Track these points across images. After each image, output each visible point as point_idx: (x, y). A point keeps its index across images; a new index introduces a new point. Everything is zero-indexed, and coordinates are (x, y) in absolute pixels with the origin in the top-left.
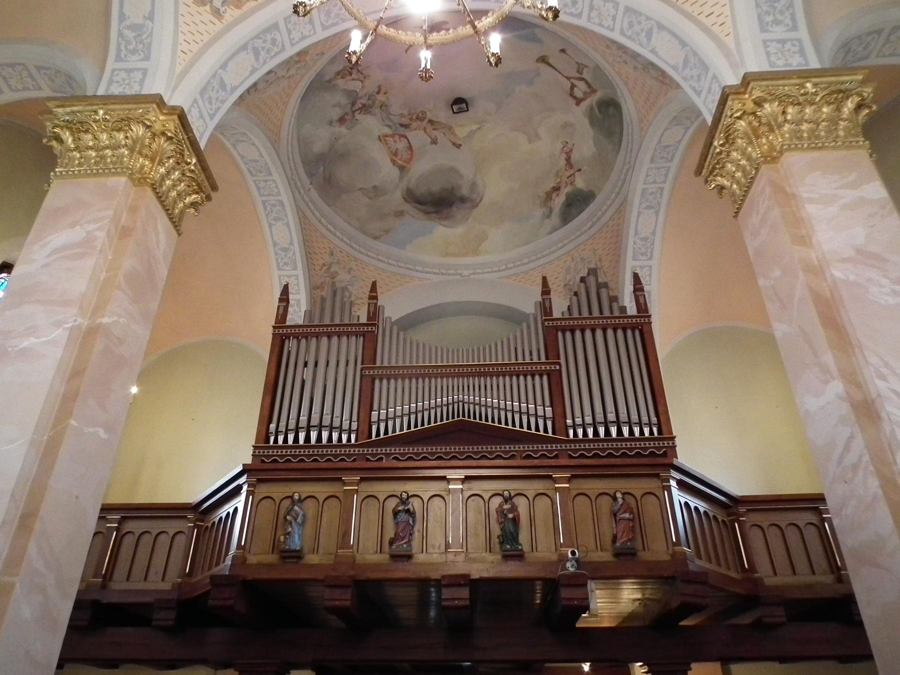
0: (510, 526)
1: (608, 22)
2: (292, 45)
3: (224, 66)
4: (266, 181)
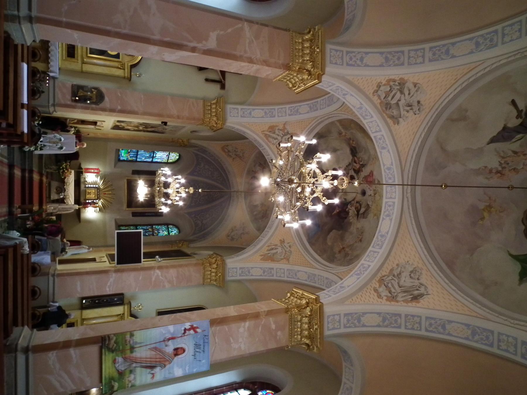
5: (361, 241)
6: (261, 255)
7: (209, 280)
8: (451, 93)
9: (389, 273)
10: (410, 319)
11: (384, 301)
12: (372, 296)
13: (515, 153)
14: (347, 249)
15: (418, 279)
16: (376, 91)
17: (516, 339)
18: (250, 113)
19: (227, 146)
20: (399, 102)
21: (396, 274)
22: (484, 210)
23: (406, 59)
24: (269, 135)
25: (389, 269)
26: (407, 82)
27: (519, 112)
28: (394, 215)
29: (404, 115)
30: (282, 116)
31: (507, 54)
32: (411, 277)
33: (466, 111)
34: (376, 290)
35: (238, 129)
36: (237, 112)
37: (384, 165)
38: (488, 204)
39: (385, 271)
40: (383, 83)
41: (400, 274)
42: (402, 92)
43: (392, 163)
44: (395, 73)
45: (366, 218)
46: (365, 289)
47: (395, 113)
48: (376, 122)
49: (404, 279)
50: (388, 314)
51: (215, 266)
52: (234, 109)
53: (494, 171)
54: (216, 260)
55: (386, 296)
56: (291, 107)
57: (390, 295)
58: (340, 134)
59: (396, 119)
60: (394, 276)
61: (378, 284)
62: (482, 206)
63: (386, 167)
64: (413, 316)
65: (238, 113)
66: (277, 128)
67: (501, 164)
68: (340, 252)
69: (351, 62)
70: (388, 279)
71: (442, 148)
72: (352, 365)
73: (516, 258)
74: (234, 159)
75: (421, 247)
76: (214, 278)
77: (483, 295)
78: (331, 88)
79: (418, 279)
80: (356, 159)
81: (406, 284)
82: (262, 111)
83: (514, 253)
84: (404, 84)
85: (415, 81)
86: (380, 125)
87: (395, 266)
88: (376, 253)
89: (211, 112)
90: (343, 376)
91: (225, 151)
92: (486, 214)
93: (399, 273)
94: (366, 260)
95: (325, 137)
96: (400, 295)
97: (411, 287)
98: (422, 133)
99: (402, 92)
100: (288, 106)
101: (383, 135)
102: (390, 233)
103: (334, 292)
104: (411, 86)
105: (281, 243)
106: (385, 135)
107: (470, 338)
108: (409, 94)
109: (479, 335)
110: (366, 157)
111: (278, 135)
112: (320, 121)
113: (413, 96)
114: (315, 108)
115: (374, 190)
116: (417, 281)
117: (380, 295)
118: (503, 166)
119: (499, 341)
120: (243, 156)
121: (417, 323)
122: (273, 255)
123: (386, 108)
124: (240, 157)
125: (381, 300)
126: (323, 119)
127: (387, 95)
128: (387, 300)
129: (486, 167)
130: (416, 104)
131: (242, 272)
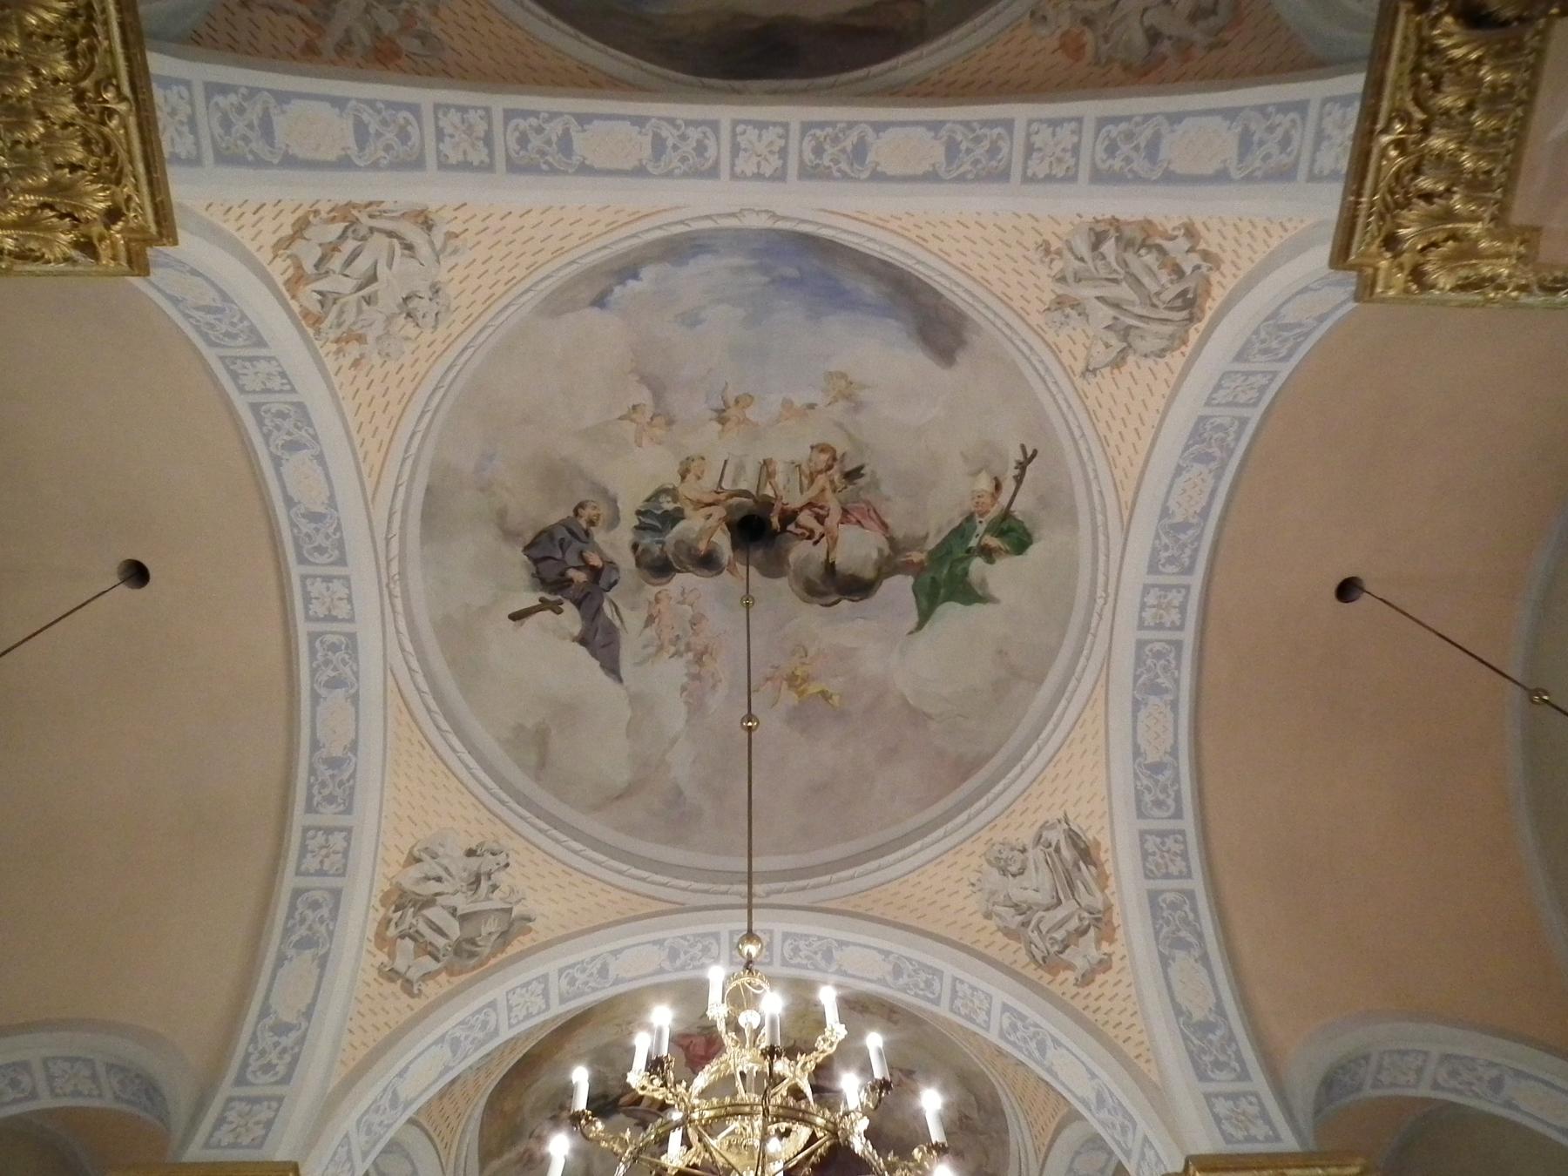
0: (128, 19)
1: (450, 120)
2: (1079, 120)
3: (1221, 177)
8: (462, 761)
9: (1018, 939)
10: (1157, 865)
11: (1118, 949)
12: (1108, 991)
13: (650, 620)
15: (1024, 851)
17: (1146, 589)
20: (459, 912)
21: (1020, 918)
22: (801, 694)
23: (335, 627)
25: (1006, 940)
26: (398, 885)
27: (544, 605)
28: (825, 932)
31: (382, 605)
32: (1021, 872)
34: (1086, 979)
37: (661, 971)
39: (1015, 953)
40: (385, 959)
41: (1016, 906)
42: (429, 902)
43: (654, 943)
44: (360, 914)
46: (1088, 1014)
47: (492, 926)
48: (513, 990)
49: (1030, 893)
50: (1157, 933)
53: (695, 669)
57: (1092, 933)
59: (513, 926)
60: (1025, 924)
61: (1062, 975)
62: (790, 698)
63: (667, 965)
64: (1145, 855)
67: (677, 654)
69: (281, 1069)
70: (1041, 945)
71: (618, 798)
72: (1367, 1058)
73: (925, 616)
75: (921, 849)
77: (1039, 680)
79: (1024, 851)
81: (1048, 886)
83: (914, 618)
84: (403, 893)
87: (991, 924)
88: (958, 986)
90: (1411, 1092)
92: (813, 688)
94: (988, 1023)
97: (1053, 870)
98: (568, 848)
99: (429, 902)
101: (561, 971)
102: (886, 945)
103: (1124, 1130)
104: (415, 872)
106: (562, 963)
107: (1169, 697)
108: (439, 879)
109: (1157, 676)
113: (446, 869)
116: (1030, 854)
117: (1101, 962)
118: (682, 648)
119: (1160, 626)
121: (1163, 843)
123: (472, 955)
125: (1115, 959)
128: (1111, 941)
129: (684, 689)
130: (473, 863)
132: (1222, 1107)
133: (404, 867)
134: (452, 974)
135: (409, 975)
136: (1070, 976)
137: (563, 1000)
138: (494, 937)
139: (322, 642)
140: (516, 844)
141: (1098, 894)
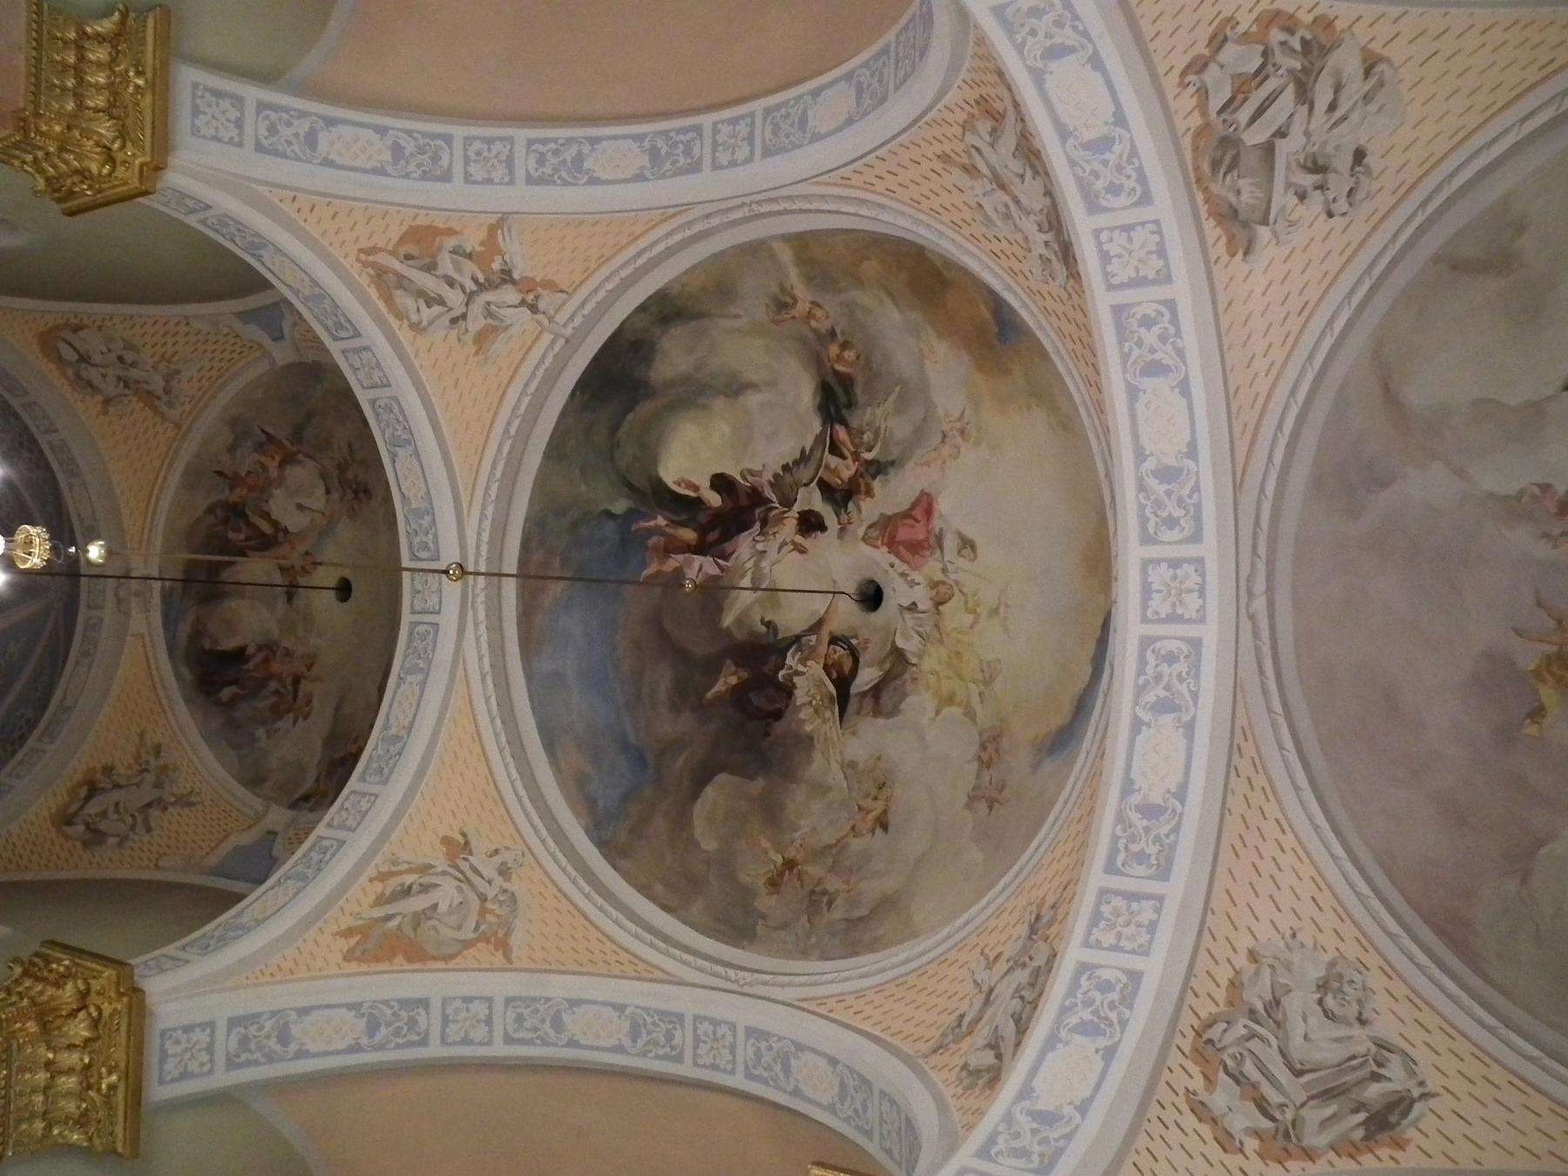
4: (750, 139)
5: (883, 823)
6: (348, 933)
7: (39, 1125)
8: (1507, 131)
12: (1192, 1144)
14: (813, 871)
15: (1362, 1021)
16: (1199, 65)
18: (311, 139)
19: (77, 329)
20: (1279, 143)
21: (1259, 1006)
22: (1537, 673)
24: (401, 277)
25: (1224, 983)
26: (1337, 44)
29: (1283, 209)
30: (488, 181)
32: (1330, 1015)
33: (1520, 228)
35: (224, 220)
36: (234, 114)
38: (1555, 649)
40: (1241, 29)
42: (1304, 94)
45: (893, 713)
47: (1247, 193)
51: (79, 1029)
52: (219, 94)
54: (84, 995)
55: (1257, 1134)
56: (544, 141)
57: (1266, 1124)
58: (782, 305)
59: (1239, 227)
60: (1252, 1013)
61: (1195, 1070)
63: (1150, 464)
65: (239, 124)
66: (450, 243)
68: (774, 884)
71: (1386, 389)
74: (107, 401)
76: (70, 1106)
78: (201, 216)
79: (1362, 1021)
80: (842, 433)
81: (1318, 1056)
82: (374, 137)
84: (1325, 51)
85: (1376, 47)
86: (1176, 253)
87: (1241, 961)
88: (1148, 905)
89: (81, 81)
91: (59, 360)
93: (1268, 997)
95: (700, 315)
96: (1314, 1115)
97: (1342, 1066)
99: (1304, 94)
100: (522, 134)
105: (452, 857)
108: (1332, 107)
110: (899, 427)
111: (451, 283)
112: (698, 228)
113: (1344, 118)
114: (682, 161)
115: (934, 585)
116: (1357, 1031)
120: (167, 391)
122: (416, 925)
123: (1215, 164)
124: (149, 397)
126: (715, 221)
127: (1242, 88)
129: (1546, 488)
130: (1344, 162)
131: (244, 1042)
132: (201, 1037)
133: (1364, 49)
134: (1198, 134)
135: (1213, 67)
136: (1198, 1083)
137: (373, 402)
138: (1232, 198)
139: (693, 139)
140: (1359, 229)
141: (1323, 1140)
